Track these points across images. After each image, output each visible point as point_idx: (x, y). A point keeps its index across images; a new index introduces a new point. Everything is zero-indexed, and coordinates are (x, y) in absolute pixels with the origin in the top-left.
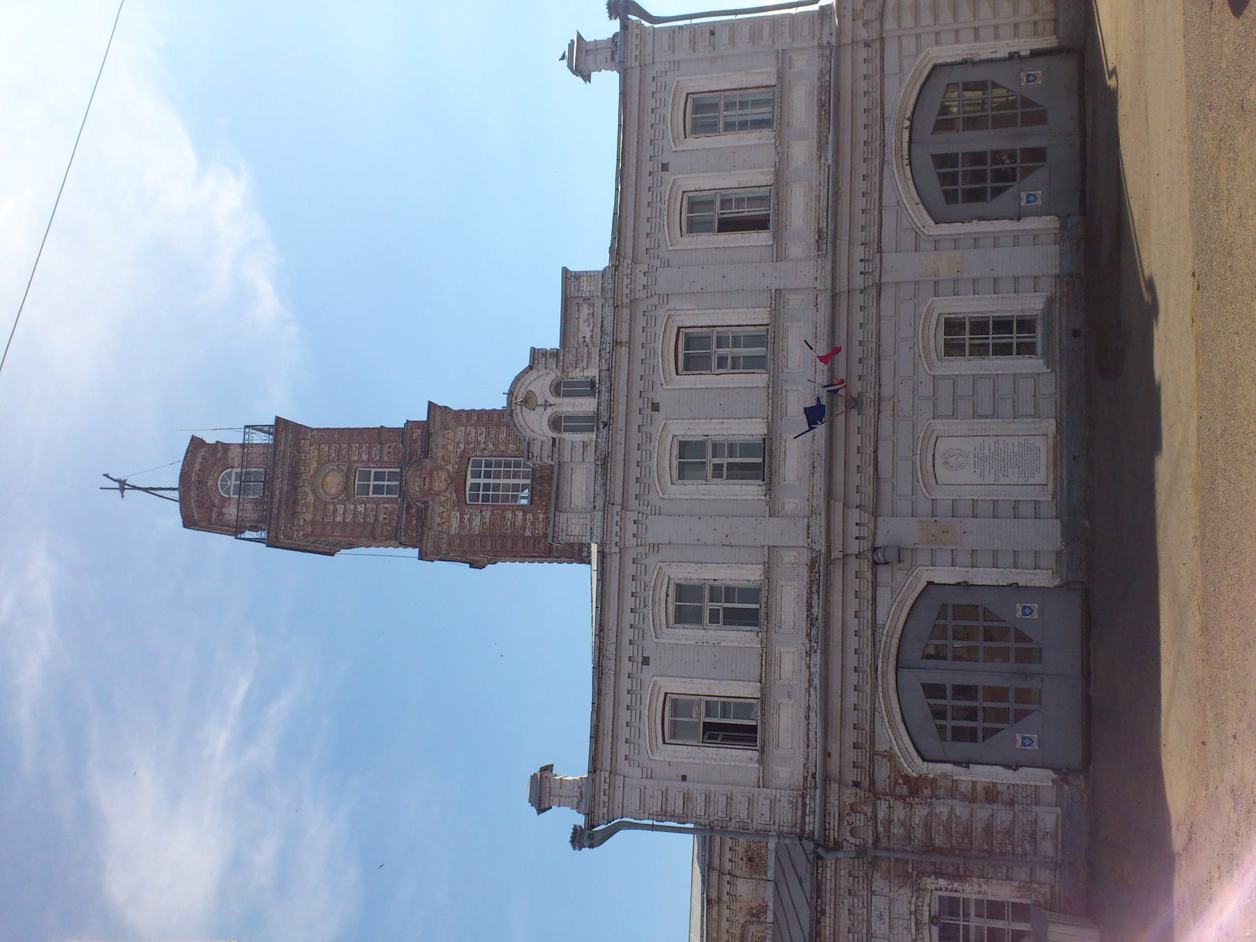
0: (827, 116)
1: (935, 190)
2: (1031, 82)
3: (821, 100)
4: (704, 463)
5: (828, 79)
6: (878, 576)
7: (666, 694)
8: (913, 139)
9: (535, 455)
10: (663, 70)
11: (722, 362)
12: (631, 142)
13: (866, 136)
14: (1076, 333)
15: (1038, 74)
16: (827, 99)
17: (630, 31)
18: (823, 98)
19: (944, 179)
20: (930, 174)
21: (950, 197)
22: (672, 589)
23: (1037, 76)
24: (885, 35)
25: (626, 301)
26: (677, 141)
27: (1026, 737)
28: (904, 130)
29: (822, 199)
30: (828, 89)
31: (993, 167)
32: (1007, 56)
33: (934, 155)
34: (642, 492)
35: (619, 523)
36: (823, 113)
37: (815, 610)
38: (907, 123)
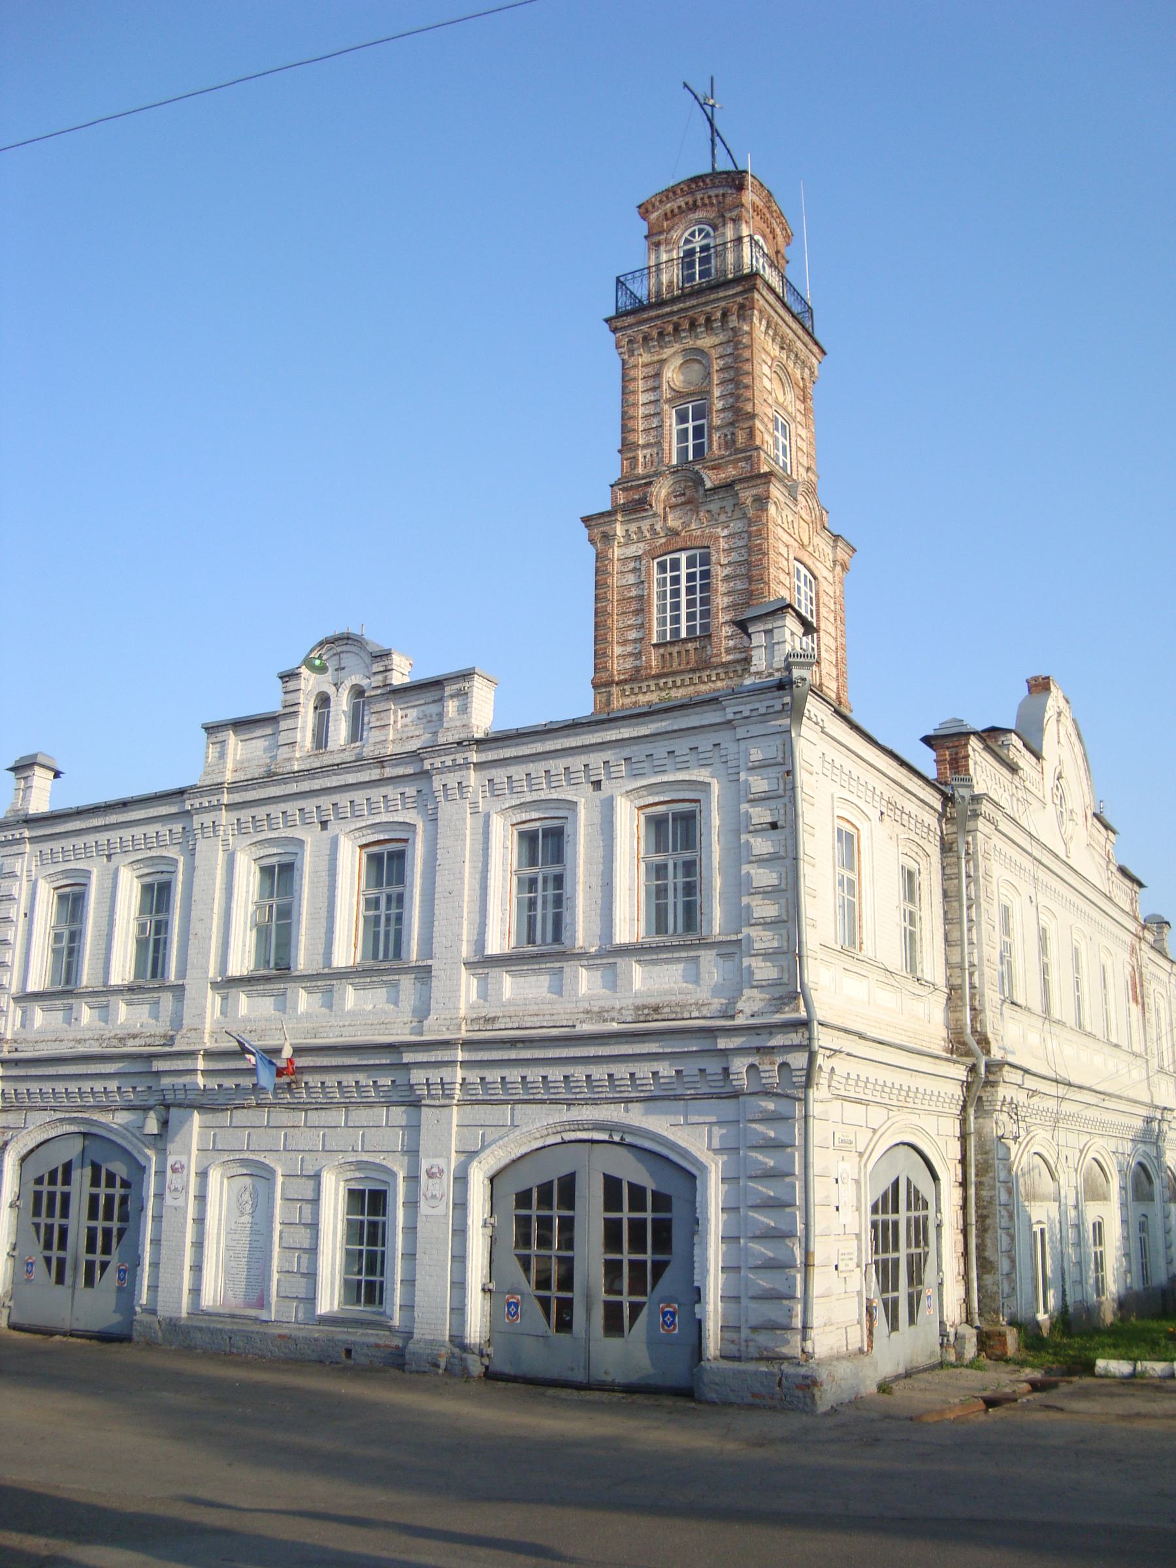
0: (642, 1018)
1: (531, 1179)
2: (663, 1318)
3: (663, 1007)
4: (151, 913)
5: (694, 1015)
6: (638, 1105)
7: (699, 801)
8: (595, 1145)
9: (288, 684)
10: (729, 758)
11: (659, 871)
12: (622, 730)
13: (491, 1080)
14: (349, 1352)
15: (674, 1329)
16: (666, 1017)
17: (777, 693)
18: (667, 1010)
19: (545, 1190)
20: (553, 1172)
21: (523, 1199)
22: (557, 823)
23: (672, 1327)
24: (741, 1098)
25: (427, 766)
26: (357, 834)
27: (674, 1318)
28: (621, 1134)
29: (535, 1019)
30: (679, 1016)
31: (554, 1261)
32: (696, 1284)
33: (574, 1180)
34: (678, 760)
35: (755, 713)
36: (646, 1011)
37: (130, 1042)
38: (617, 1138)
